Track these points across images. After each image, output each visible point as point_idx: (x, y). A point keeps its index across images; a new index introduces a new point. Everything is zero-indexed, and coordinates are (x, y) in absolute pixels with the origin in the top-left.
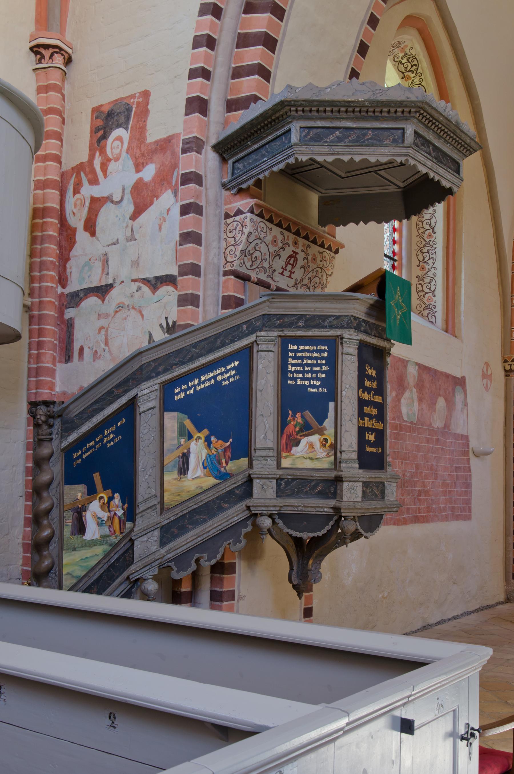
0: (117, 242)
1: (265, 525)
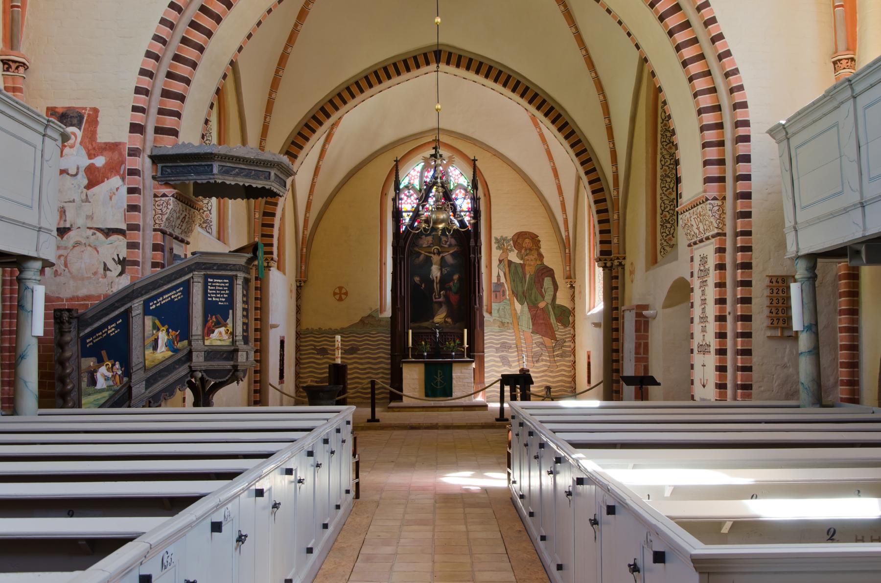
0: (74, 201)
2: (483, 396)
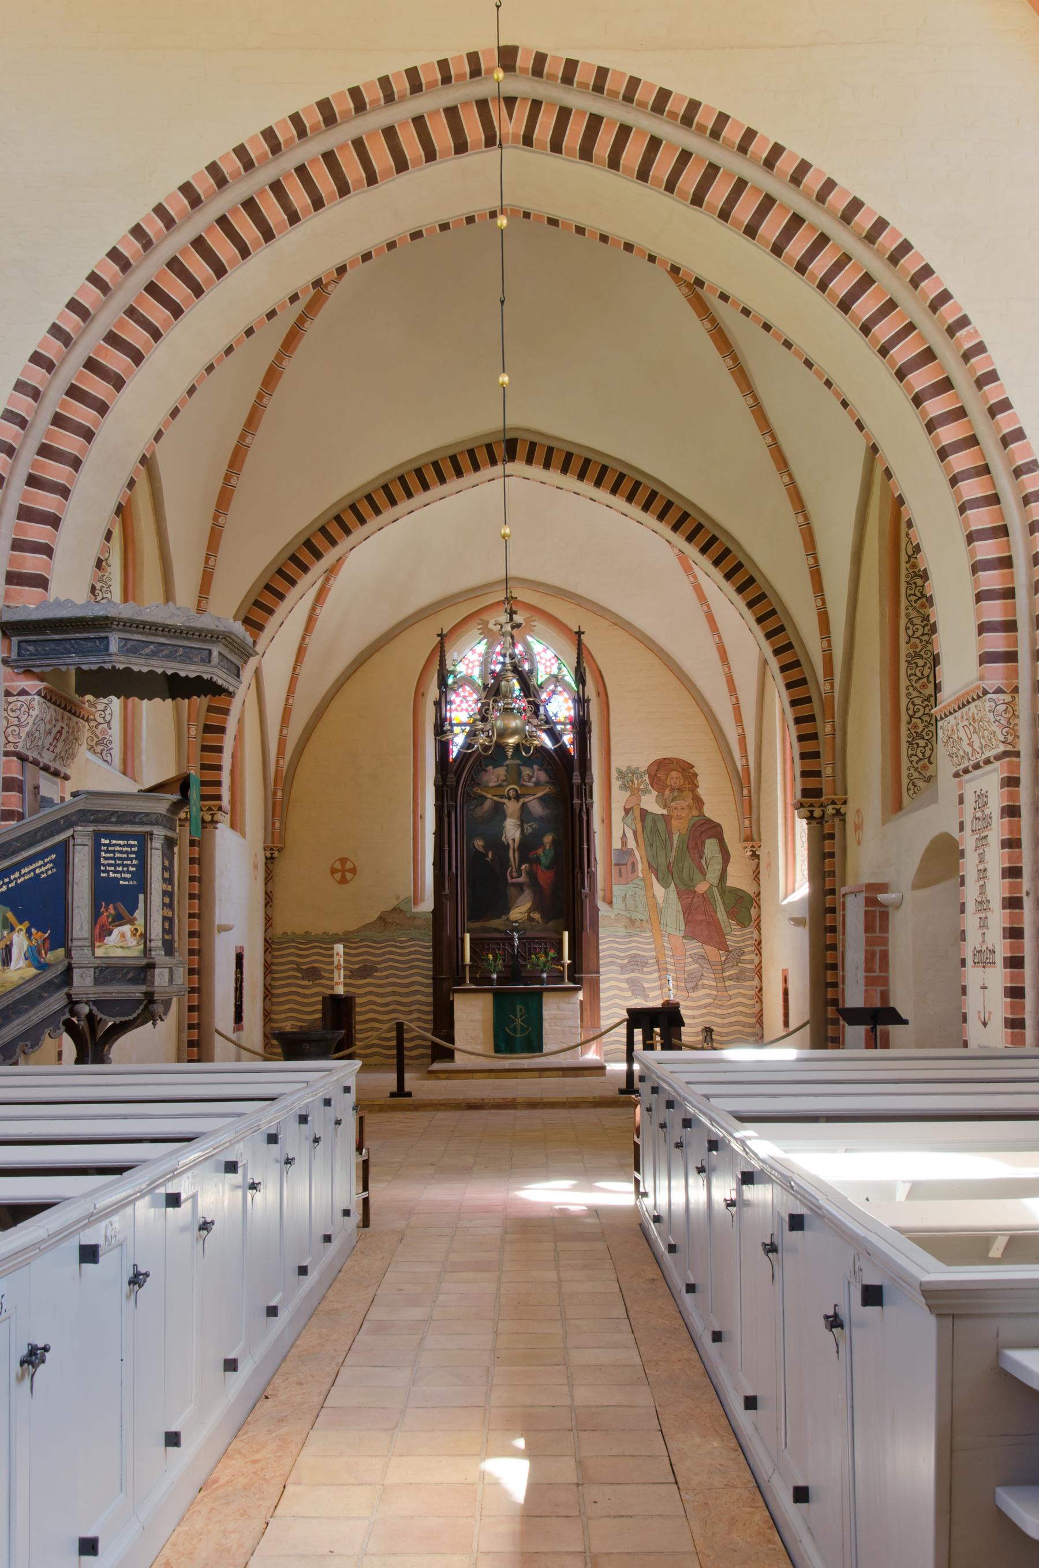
2: (598, 1051)
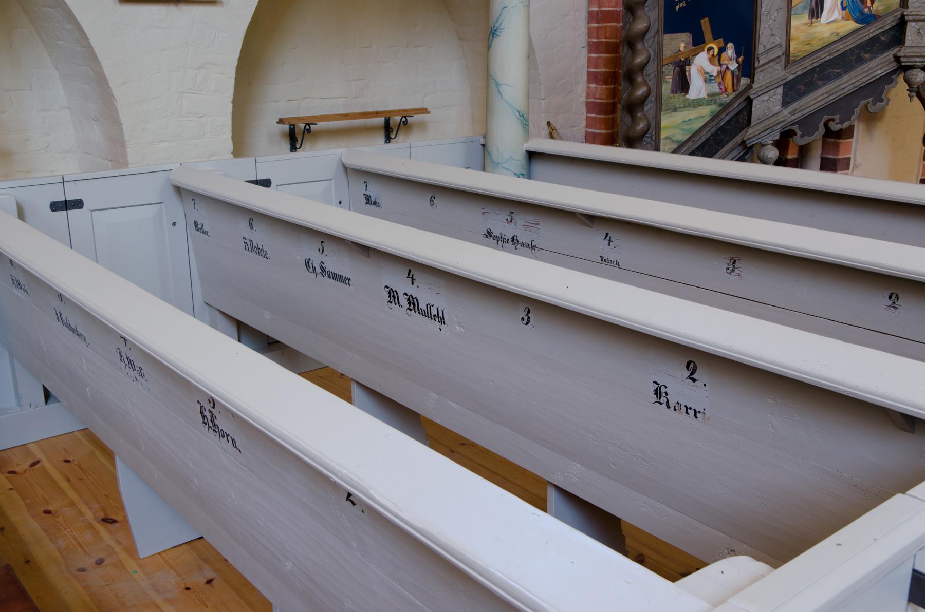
1: (918, 80)
